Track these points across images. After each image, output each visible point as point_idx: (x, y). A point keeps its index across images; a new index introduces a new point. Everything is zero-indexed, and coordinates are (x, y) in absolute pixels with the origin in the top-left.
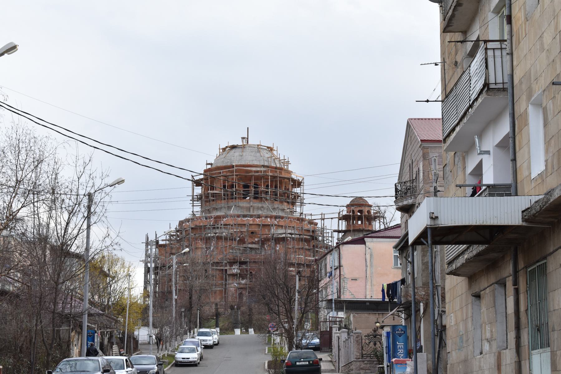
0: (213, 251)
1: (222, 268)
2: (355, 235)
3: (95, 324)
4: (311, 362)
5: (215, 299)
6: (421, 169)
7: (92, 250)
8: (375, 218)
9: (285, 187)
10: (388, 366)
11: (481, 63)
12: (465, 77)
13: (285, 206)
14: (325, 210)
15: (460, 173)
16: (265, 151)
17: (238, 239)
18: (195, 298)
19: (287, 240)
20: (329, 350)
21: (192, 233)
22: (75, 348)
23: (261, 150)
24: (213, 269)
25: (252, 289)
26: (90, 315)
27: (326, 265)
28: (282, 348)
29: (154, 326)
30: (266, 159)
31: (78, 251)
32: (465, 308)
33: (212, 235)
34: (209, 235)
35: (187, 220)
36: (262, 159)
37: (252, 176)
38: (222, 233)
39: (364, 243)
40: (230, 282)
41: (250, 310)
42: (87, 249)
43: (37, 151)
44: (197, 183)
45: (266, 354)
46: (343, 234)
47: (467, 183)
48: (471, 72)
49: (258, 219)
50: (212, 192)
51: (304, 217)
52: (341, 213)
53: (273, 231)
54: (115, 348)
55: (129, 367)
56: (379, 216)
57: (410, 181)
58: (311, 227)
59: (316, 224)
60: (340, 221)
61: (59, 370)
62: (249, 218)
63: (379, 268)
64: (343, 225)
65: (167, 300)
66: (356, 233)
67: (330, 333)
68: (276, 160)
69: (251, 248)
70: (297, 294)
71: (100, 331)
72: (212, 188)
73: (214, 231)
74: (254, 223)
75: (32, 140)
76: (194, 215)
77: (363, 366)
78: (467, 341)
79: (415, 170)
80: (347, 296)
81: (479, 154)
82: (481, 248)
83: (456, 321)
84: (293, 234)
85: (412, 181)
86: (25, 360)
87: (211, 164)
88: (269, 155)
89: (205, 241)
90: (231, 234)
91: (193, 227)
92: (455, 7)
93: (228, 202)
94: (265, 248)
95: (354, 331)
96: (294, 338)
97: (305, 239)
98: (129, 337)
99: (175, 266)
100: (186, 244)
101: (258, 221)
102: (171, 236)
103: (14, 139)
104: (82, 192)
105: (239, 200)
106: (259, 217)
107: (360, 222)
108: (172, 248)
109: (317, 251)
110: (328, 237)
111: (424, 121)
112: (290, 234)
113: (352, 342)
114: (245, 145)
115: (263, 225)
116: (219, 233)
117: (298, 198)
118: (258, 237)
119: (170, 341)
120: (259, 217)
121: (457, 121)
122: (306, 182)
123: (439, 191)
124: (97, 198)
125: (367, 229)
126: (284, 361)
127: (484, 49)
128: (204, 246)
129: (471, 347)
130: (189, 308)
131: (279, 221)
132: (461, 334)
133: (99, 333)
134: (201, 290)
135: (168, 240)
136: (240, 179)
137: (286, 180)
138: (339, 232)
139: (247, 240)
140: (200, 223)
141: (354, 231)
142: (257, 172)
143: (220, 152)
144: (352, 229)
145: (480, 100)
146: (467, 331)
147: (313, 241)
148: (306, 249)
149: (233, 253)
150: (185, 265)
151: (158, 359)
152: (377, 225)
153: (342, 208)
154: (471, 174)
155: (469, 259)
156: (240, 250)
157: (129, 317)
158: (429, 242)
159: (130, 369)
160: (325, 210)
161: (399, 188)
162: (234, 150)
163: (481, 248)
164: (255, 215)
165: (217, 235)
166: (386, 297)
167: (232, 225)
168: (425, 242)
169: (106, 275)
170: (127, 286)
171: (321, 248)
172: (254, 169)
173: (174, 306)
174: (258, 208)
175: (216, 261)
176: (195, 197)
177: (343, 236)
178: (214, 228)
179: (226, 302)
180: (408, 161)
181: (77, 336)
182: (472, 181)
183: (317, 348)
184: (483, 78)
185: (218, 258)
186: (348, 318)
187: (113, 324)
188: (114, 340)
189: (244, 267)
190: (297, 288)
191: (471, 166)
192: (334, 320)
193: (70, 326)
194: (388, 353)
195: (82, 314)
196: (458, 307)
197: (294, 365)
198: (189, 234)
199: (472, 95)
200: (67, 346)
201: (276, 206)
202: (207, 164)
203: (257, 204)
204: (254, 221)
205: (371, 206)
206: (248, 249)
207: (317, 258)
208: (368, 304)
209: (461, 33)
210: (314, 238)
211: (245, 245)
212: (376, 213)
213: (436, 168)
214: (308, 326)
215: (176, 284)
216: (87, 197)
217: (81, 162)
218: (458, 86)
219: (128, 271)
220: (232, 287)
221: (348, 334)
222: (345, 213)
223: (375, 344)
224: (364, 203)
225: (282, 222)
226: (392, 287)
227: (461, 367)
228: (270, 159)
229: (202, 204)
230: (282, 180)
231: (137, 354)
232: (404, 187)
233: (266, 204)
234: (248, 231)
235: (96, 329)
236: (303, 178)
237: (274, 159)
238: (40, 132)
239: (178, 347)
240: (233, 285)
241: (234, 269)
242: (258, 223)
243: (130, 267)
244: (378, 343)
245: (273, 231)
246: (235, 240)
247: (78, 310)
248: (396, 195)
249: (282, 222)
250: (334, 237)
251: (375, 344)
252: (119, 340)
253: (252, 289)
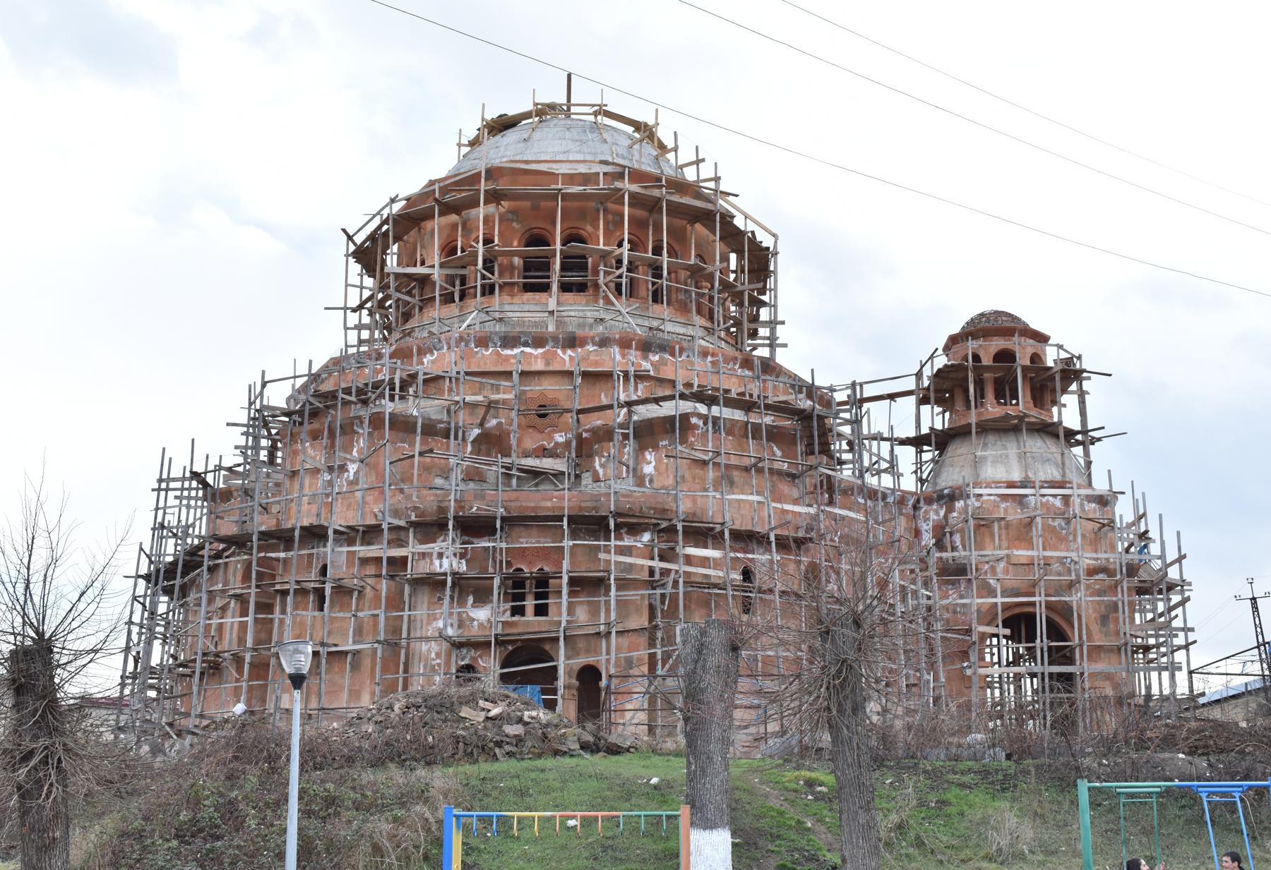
2: (985, 445)
5: (355, 694)
17: (477, 431)
40: (421, 612)
49: (569, 352)
62: (528, 350)
64: (934, 418)
74: (551, 368)
94: (596, 473)
101: (566, 358)
105: (507, 298)
115: (585, 375)
136: (510, 216)
148: (780, 473)
204: (547, 358)
220: (427, 639)
241: (440, 556)
242: (567, 367)
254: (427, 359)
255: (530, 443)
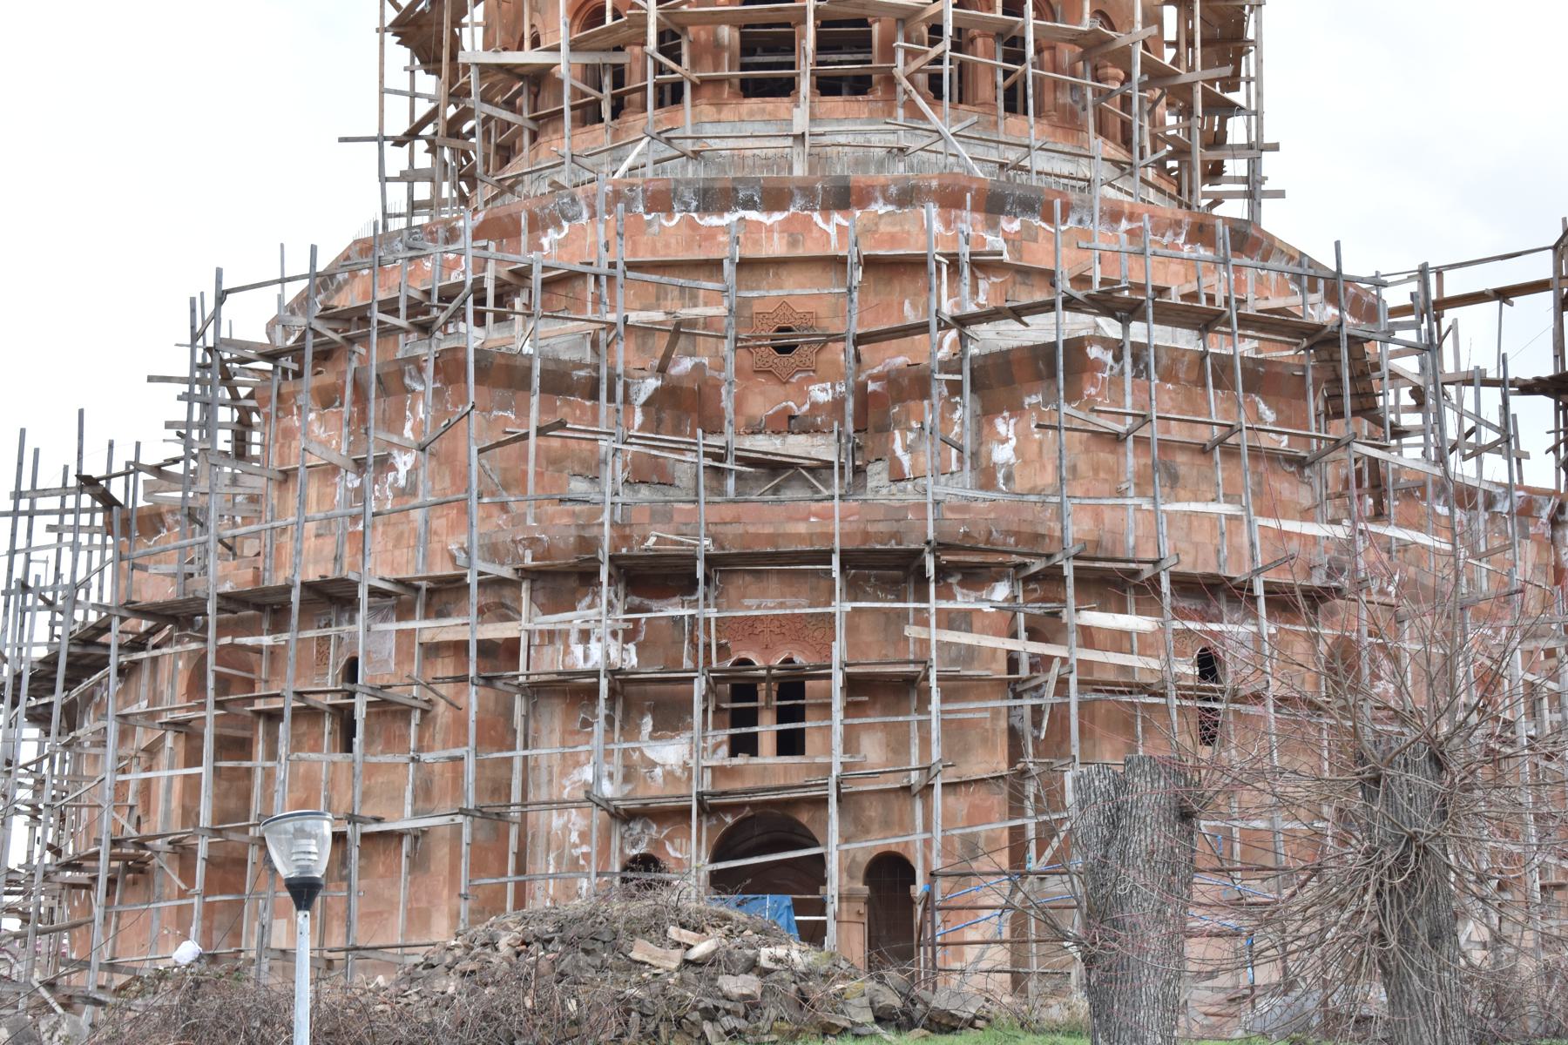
5: (419, 918)
17: (652, 384)
20: (1047, 540)
40: (547, 751)
49: (837, 218)
62: (752, 215)
74: (800, 252)
94: (895, 465)
105: (707, 111)
115: (872, 264)
148: (1273, 456)
200: (1212, 972)
204: (792, 231)
241: (585, 636)
242: (834, 249)
254: (550, 238)
255: (762, 405)
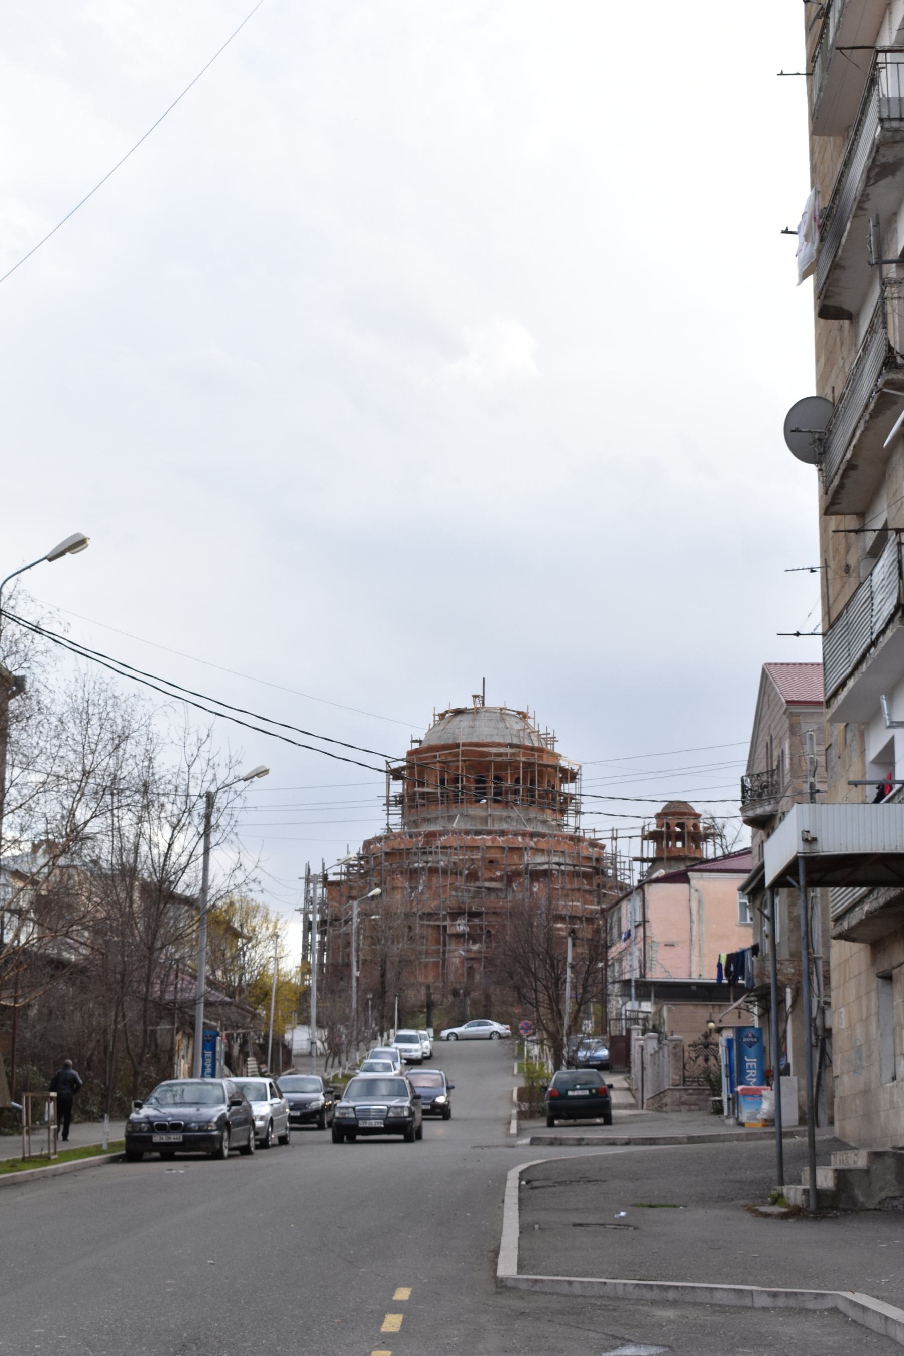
0: (422, 893)
1: (437, 923)
2: (670, 866)
3: (216, 1020)
4: (594, 1091)
5: (426, 977)
6: (787, 752)
7: (212, 892)
8: (706, 837)
9: (549, 782)
10: (729, 1099)
11: (892, 568)
12: (863, 593)
13: (548, 815)
14: (617, 823)
15: (856, 760)
16: (514, 719)
17: (466, 872)
18: (390, 975)
19: (552, 875)
20: (626, 1069)
21: (386, 861)
22: (183, 1061)
23: (507, 718)
24: (422, 926)
25: (490, 961)
26: (208, 1004)
27: (620, 919)
28: (542, 1065)
29: (320, 1025)
30: (515, 733)
31: (188, 893)
32: (864, 999)
33: (421, 865)
34: (416, 865)
35: (378, 839)
36: (511, 733)
37: (490, 762)
38: (438, 862)
39: (686, 880)
40: (453, 947)
41: (488, 997)
42: (204, 890)
43: (119, 721)
44: (396, 774)
45: (514, 1075)
46: (650, 864)
47: (868, 778)
48: (873, 584)
49: (502, 838)
50: (420, 790)
51: (581, 834)
52: (646, 828)
53: (527, 858)
54: (252, 1062)
55: (275, 1097)
56: (713, 833)
57: (767, 772)
58: (593, 852)
59: (603, 847)
60: (645, 842)
61: (153, 1101)
62: (485, 836)
63: (714, 926)
64: (650, 849)
65: (341, 979)
66: (673, 863)
67: (627, 1039)
68: (532, 735)
69: (489, 889)
70: (569, 971)
71: (224, 1033)
72: (422, 784)
73: (425, 858)
75: (110, 702)
76: (389, 830)
77: (685, 1097)
78: (869, 1056)
79: (776, 754)
80: (656, 975)
81: (889, 727)
82: (894, 893)
83: (850, 1020)
84: (562, 864)
85: (771, 773)
86: (96, 1081)
87: (420, 742)
88: (520, 726)
89: (408, 876)
90: (455, 863)
91: (388, 850)
92: (845, 470)
93: (448, 807)
95: (670, 1037)
96: (563, 1048)
97: (584, 872)
98: (276, 1043)
99: (356, 920)
100: (375, 880)
102: (349, 866)
103: (80, 700)
104: (194, 791)
105: (469, 805)
106: (503, 833)
107: (679, 844)
108: (351, 888)
109: (605, 894)
110: (624, 869)
111: (791, 667)
112: (559, 864)
113: (666, 1055)
114: (478, 708)
115: (510, 849)
116: (433, 862)
117: (570, 802)
118: (500, 870)
119: (347, 1052)
120: (503, 833)
121: (850, 669)
122: (585, 775)
123: (818, 791)
124: (221, 800)
125: (692, 855)
126: (546, 1088)
127: (895, 543)
128: (407, 885)
129: (876, 1068)
130: (381, 993)
131: (539, 841)
132: (858, 1043)
133: (224, 1036)
134: (400, 961)
135: (344, 874)
137: (549, 769)
138: (643, 860)
139: (482, 874)
140: (399, 844)
141: (670, 859)
142: (500, 755)
143: (435, 721)
144: (665, 856)
145: (889, 633)
146: (868, 1040)
147: (597, 877)
148: (585, 891)
149: (457, 896)
150: (373, 917)
151: (326, 1082)
152: (709, 850)
153: (648, 821)
154: (876, 762)
155: (871, 912)
156: (469, 891)
157: (276, 1009)
158: (802, 882)
159: (277, 1100)
160: (617, 823)
161: (748, 785)
162: (459, 718)
163: (894, 893)
164: (496, 832)
165: (429, 865)
166: (724, 977)
167: (456, 849)
168: (794, 883)
169: (237, 935)
170: (272, 953)
171: (611, 889)
172: (494, 750)
173: (354, 989)
174: (502, 819)
175: (427, 910)
176: (391, 798)
177: (650, 868)
178: (424, 853)
179: (444, 983)
180: (764, 738)
181: (185, 1042)
182: (877, 775)
183: (604, 1066)
184: (896, 595)
185: (432, 905)
186: (659, 1013)
187: (248, 1020)
188: (250, 1048)
189: (476, 921)
190: (569, 960)
191: (874, 749)
192: (633, 1015)
193: (173, 1024)
194: (730, 1075)
195: (194, 1003)
196: (852, 997)
197: (564, 1096)
198: (380, 863)
199: (875, 624)
201: (532, 815)
202: (413, 741)
203: (499, 811)
204: (493, 840)
205: (698, 816)
206: (483, 890)
207: (604, 906)
208: (694, 988)
209: (855, 516)
210: (599, 871)
211: (478, 884)
212: (708, 828)
213: (814, 751)
214: (588, 1025)
215: (357, 951)
216: (204, 799)
217: (192, 739)
218: (851, 608)
219: (275, 928)
221: (660, 1042)
222: (653, 828)
223: (706, 1060)
224: (686, 810)
225: (543, 844)
226: (736, 961)
227: (858, 1102)
228: (521, 733)
229: (403, 810)
230: (542, 770)
231: (290, 1074)
232: (757, 784)
233: (515, 812)
234: (483, 858)
235: (218, 1029)
236: (580, 767)
237: (529, 733)
238: (124, 686)
239: (361, 1061)
240: (458, 953)
241: (459, 925)
242: (501, 844)
243: (278, 920)
244: (712, 1058)
245: (527, 858)
246: (461, 874)
247: (187, 995)
248: (743, 797)
249: (543, 844)
250: (633, 870)
251: (706, 1060)
252: (258, 1048)
253: (490, 961)
254: (442, 838)
255: (487, 875)
